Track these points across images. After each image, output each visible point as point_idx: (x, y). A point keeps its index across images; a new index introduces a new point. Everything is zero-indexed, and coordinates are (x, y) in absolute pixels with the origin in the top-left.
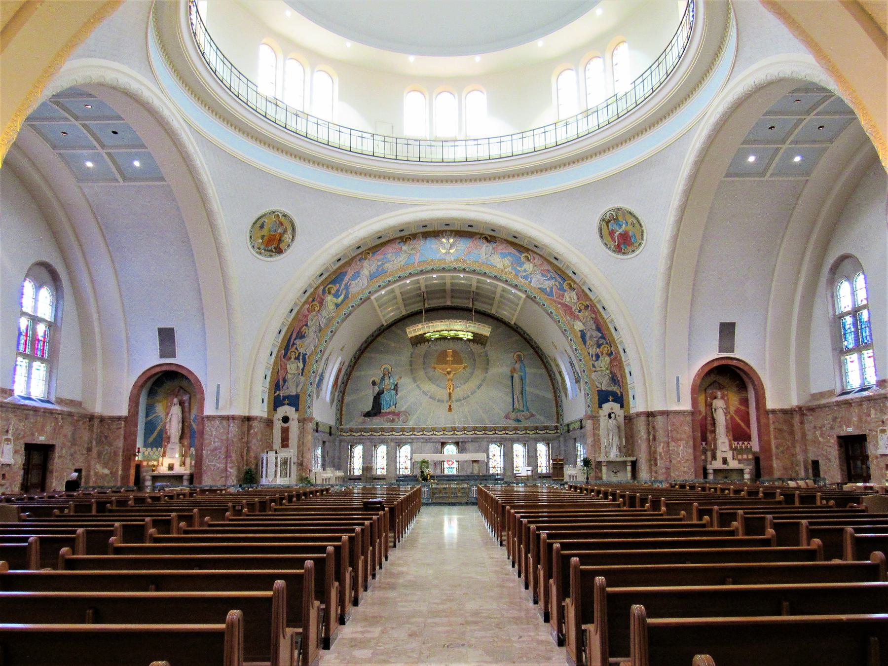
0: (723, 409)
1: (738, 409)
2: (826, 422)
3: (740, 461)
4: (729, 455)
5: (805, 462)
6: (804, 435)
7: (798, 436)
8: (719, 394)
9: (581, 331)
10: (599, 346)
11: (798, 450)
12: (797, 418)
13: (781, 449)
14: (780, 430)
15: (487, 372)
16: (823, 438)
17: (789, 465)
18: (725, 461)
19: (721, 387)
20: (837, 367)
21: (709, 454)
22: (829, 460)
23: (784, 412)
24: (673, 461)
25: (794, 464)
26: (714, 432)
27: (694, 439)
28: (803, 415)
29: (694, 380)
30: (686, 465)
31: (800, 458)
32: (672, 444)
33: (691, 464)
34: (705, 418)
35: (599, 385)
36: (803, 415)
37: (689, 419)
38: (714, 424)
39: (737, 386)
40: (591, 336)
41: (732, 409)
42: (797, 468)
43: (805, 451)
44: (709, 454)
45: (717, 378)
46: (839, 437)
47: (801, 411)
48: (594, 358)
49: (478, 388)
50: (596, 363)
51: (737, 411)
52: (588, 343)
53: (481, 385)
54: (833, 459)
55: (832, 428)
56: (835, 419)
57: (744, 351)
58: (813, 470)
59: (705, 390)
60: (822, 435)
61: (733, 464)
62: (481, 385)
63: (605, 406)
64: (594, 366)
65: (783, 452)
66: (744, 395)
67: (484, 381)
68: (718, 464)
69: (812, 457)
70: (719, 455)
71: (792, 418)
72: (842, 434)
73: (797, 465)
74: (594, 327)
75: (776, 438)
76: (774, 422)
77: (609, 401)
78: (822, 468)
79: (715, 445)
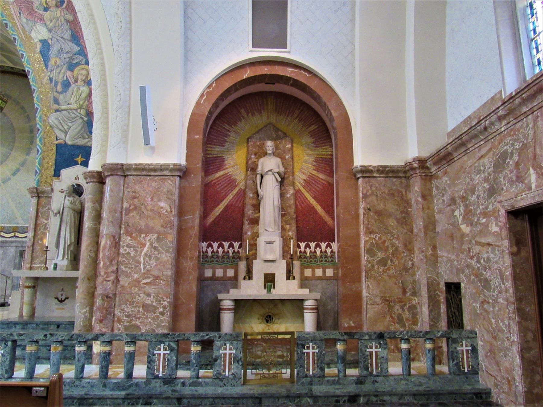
0: (271, 174)
1: (311, 176)
2: (478, 178)
3: (304, 283)
4: (280, 270)
5: (432, 286)
6: (430, 225)
7: (419, 224)
8: (269, 145)
9: (44, 42)
10: (71, 67)
11: (418, 257)
12: (417, 185)
13: (380, 255)
14: (379, 213)
15: (28, 154)
16: (471, 224)
17: (397, 292)
18: (269, 280)
19: (278, 135)
20: (506, 33)
21: (242, 265)
22: (486, 284)
23: (387, 172)
24: (124, 281)
25: (408, 290)
26: (255, 222)
27: (181, 232)
28: (428, 178)
29: (198, 103)
30: (149, 289)
31: (422, 276)
32: (126, 240)
33: (166, 288)
34: (242, 194)
35: (61, 135)
36: (428, 178)
37: (172, 185)
38: (257, 207)
39: (313, 134)
40: (61, 51)
41: (300, 178)
42: (415, 300)
43: (433, 261)
44: (242, 265)
45: (273, 120)
46: (515, 214)
47: (422, 169)
48: (59, 88)
49: (14, 174)
50: (61, 97)
51: (309, 183)
52: (52, 62)
53: (18, 170)
54: (495, 281)
55: (492, 192)
56: (500, 164)
57: (305, 48)
58: (449, 306)
59: (248, 142)
60: (468, 214)
61: (286, 288)
62: (18, 170)
63: (66, 173)
64: (56, 101)
65: (383, 262)
66: (324, 151)
67: (23, 165)
68: (252, 289)
69: (446, 275)
70: (259, 269)
71: (408, 187)
72: (525, 200)
73: (414, 294)
74: (67, 35)
75: (369, 231)
76: (365, 196)
77: (76, 163)
78: (470, 304)
79: (254, 246)
